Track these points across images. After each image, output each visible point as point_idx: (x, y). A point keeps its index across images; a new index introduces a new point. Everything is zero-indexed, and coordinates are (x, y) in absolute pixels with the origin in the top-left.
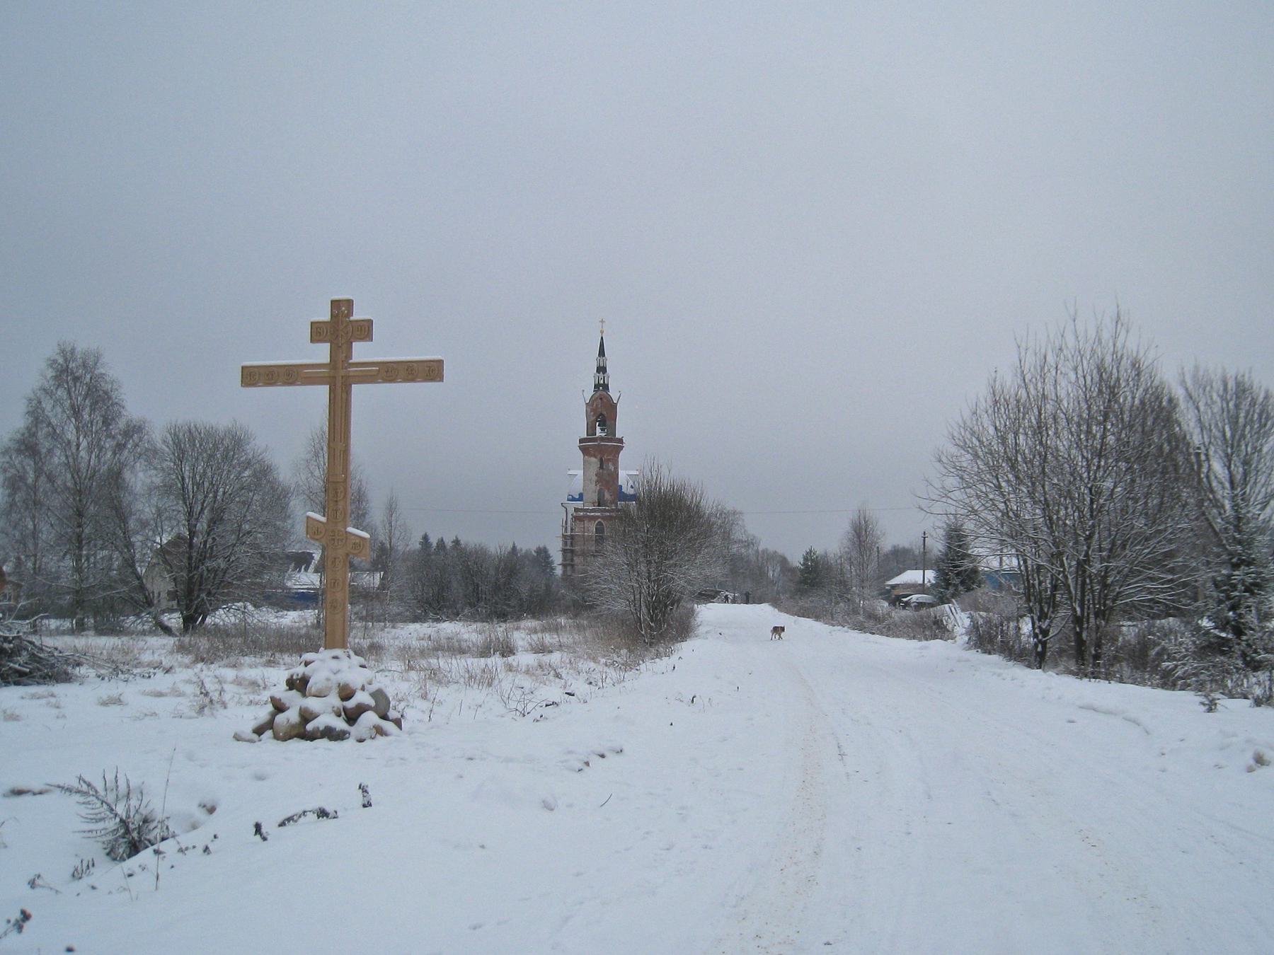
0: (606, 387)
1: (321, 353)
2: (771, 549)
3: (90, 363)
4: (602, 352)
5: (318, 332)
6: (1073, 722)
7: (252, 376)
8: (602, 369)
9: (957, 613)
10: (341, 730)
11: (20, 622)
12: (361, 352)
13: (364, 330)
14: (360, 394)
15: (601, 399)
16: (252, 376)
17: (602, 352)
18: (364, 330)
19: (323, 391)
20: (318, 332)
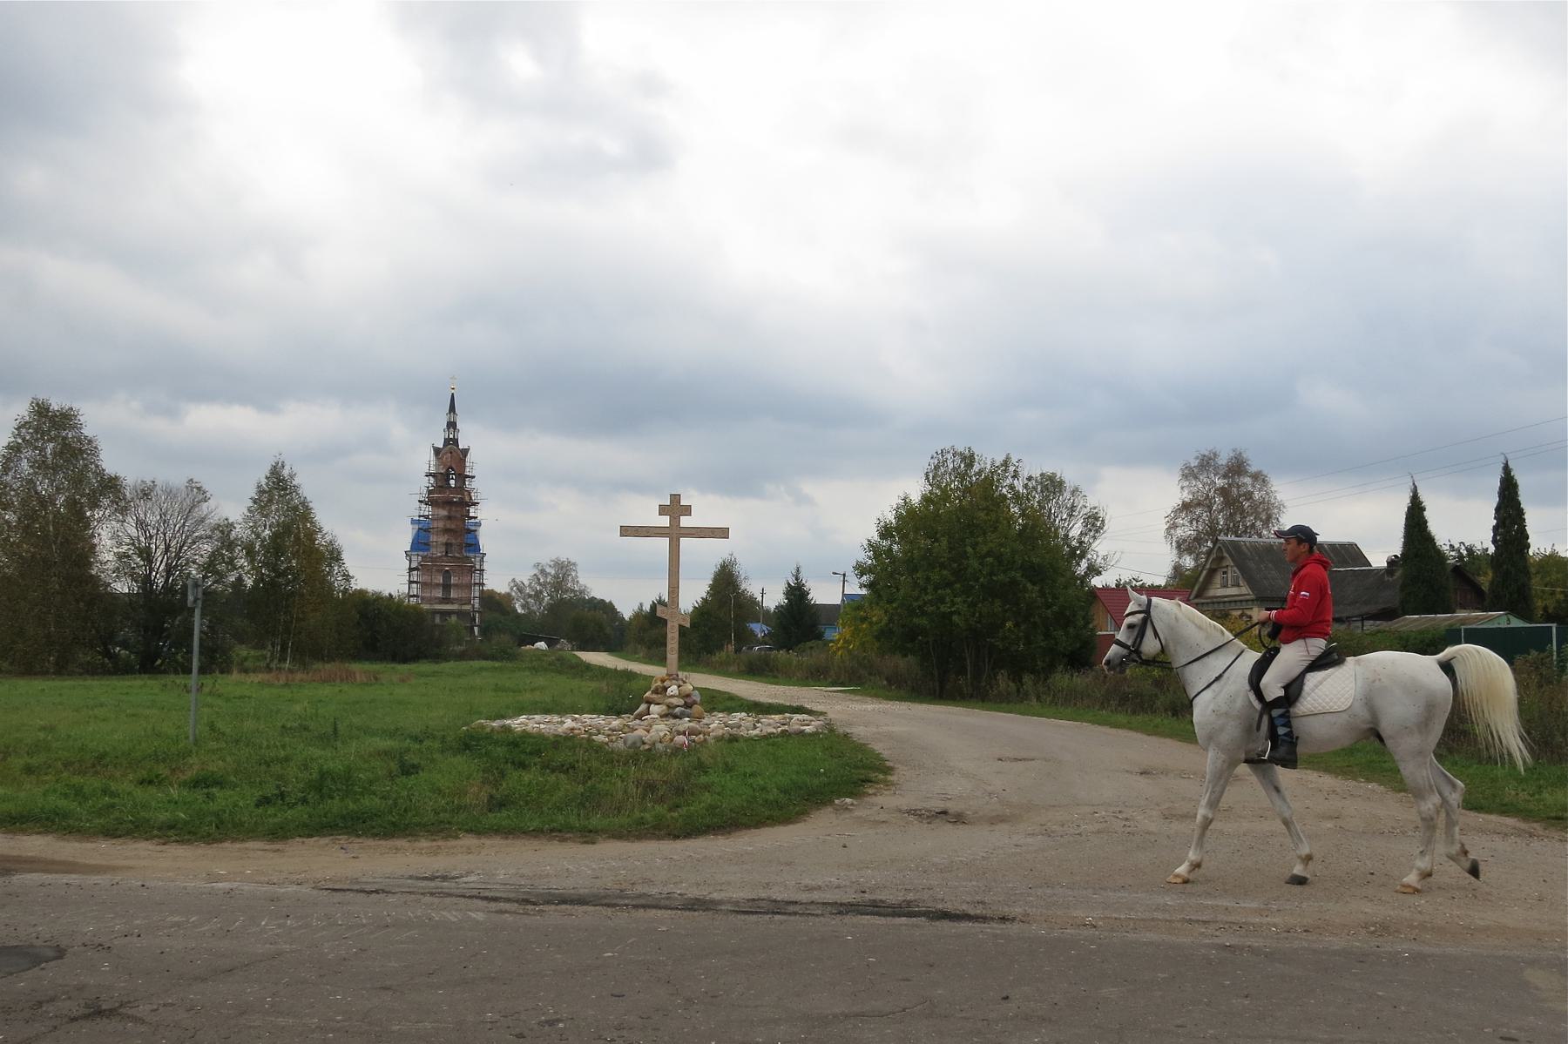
0: (456, 441)
1: (665, 521)
2: (599, 597)
3: (65, 419)
4: (452, 409)
5: (663, 510)
6: (908, 980)
7: (626, 531)
8: (452, 425)
9: (497, 689)
10: (449, 661)
11: (1433, 758)
12: (685, 522)
13: (687, 510)
14: (664, 543)
15: (451, 453)
16: (626, 531)
17: (452, 409)
18: (687, 510)
19: (664, 543)
20: (663, 510)
